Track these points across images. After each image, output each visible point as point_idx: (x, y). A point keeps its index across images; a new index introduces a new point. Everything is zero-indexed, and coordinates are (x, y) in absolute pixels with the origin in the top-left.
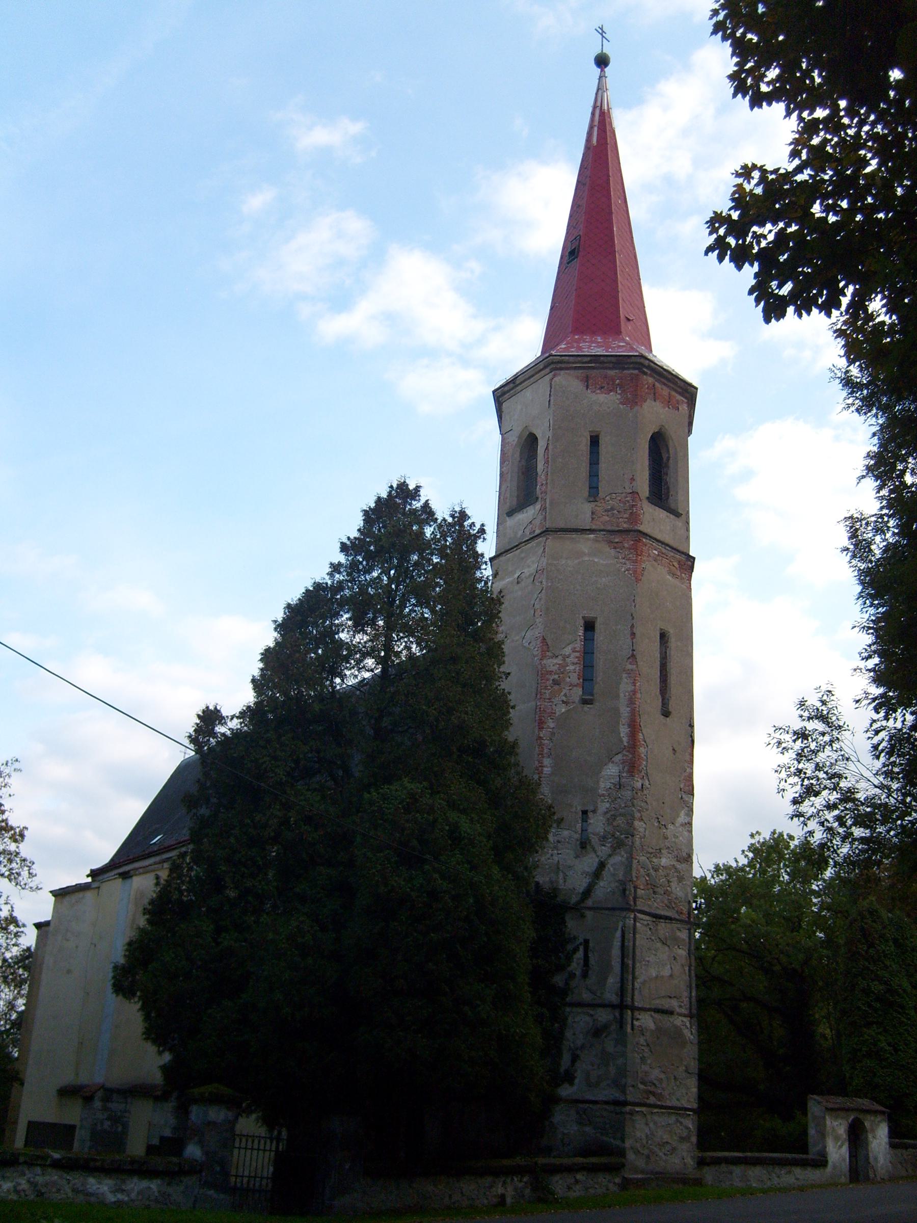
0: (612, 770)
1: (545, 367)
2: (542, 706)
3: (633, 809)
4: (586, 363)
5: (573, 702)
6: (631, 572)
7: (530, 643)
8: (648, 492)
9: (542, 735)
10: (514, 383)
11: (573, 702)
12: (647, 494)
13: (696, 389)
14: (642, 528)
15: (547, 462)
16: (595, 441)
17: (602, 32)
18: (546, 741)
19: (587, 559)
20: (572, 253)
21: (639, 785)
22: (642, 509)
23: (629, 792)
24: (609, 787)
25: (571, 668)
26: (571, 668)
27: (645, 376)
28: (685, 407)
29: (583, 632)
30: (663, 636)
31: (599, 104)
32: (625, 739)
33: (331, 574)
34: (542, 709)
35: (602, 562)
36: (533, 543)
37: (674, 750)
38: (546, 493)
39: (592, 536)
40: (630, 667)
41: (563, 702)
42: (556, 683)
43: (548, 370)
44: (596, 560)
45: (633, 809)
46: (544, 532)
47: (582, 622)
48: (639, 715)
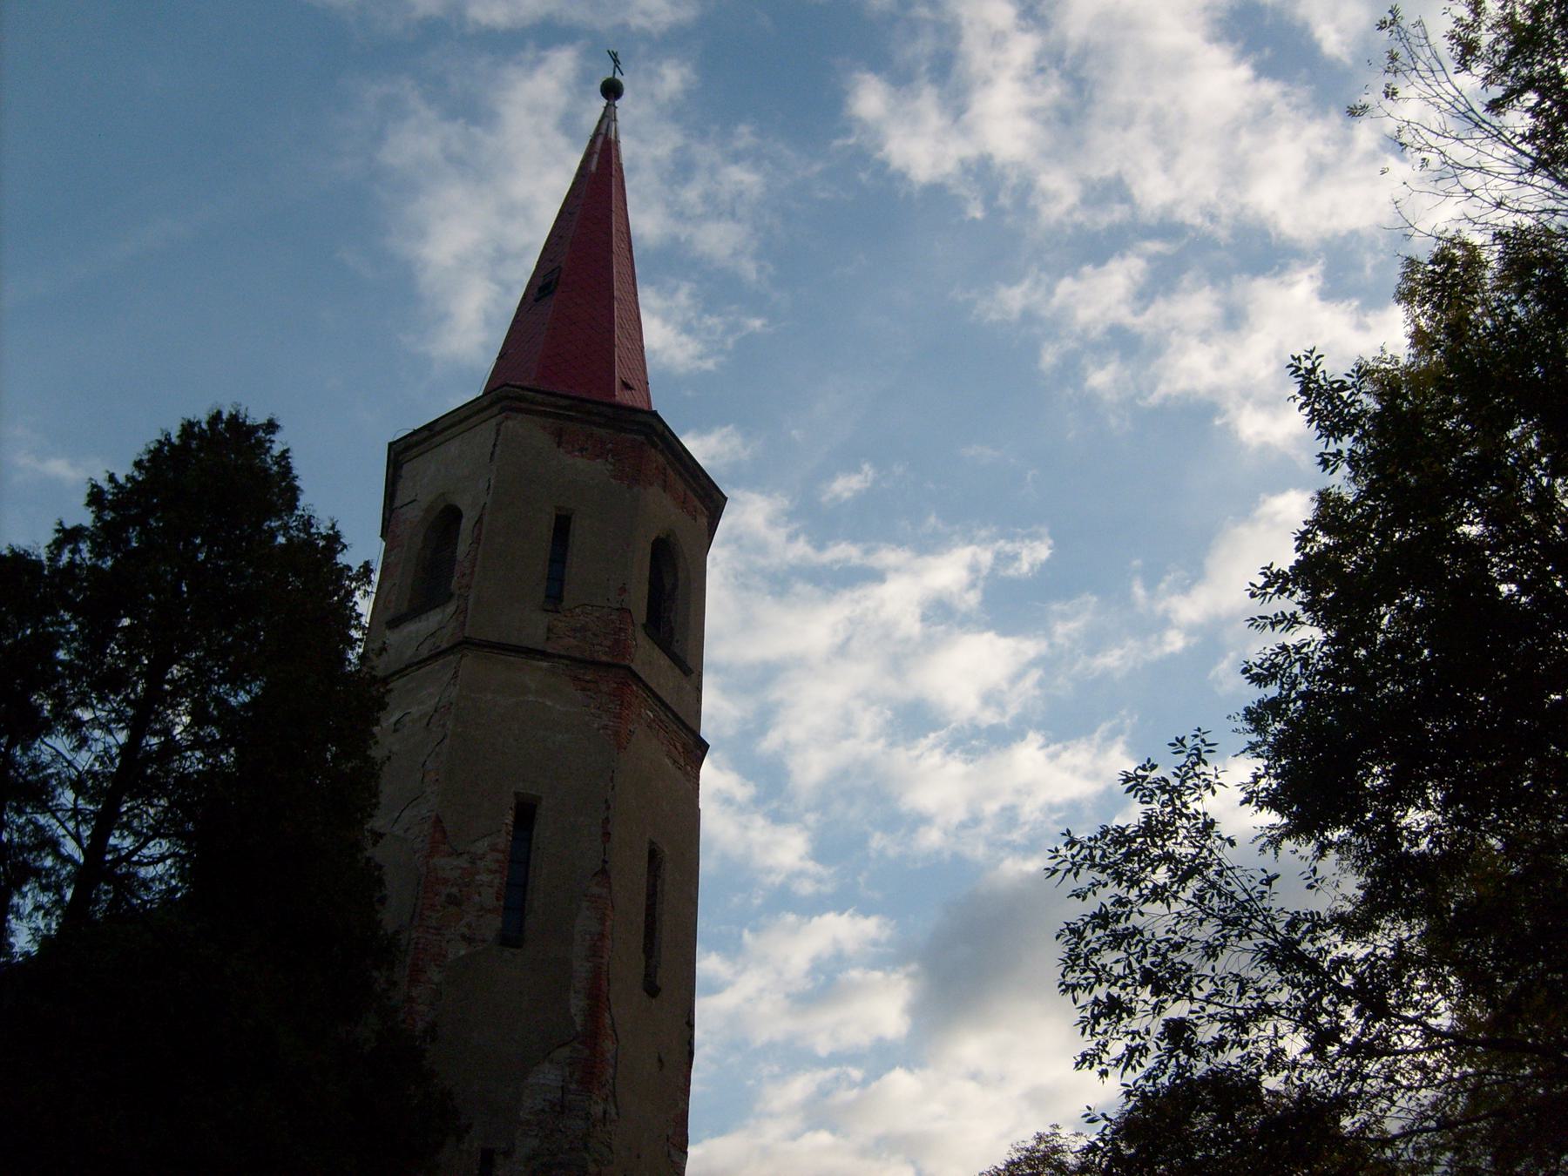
0: (548, 1077)
1: (491, 405)
2: (423, 941)
3: (587, 1156)
4: (565, 408)
5: (484, 941)
6: (610, 732)
7: (408, 829)
8: (645, 617)
9: (414, 994)
10: (430, 430)
11: (484, 941)
12: (644, 621)
13: (726, 499)
14: (633, 666)
15: (477, 540)
16: (562, 527)
17: (614, 57)
18: (421, 1008)
19: (531, 698)
20: (541, 289)
21: (597, 1110)
22: (635, 640)
23: (580, 1122)
24: (540, 1107)
25: (485, 878)
26: (485, 878)
27: (653, 450)
28: (705, 521)
29: (512, 819)
30: (654, 856)
31: (603, 131)
32: (579, 1020)
33: (57, 546)
34: (420, 946)
35: (558, 707)
36: (436, 665)
37: (660, 1060)
38: (468, 586)
39: (545, 664)
40: (596, 890)
41: (463, 937)
42: (453, 900)
43: (495, 410)
44: (549, 703)
45: (587, 1156)
46: (460, 644)
47: (512, 802)
48: (608, 980)
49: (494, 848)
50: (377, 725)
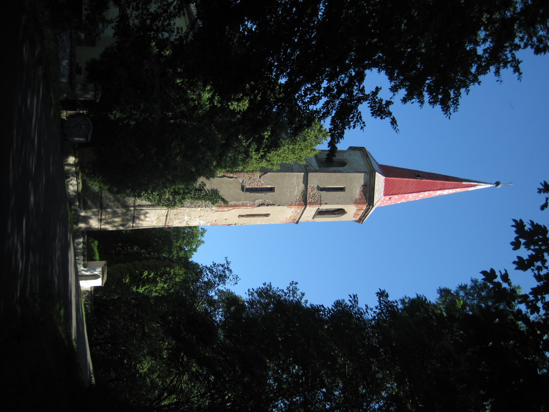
16: (342, 189)
37: (226, 219)
44: (296, 191)
49: (262, 184)
50: (123, 212)
